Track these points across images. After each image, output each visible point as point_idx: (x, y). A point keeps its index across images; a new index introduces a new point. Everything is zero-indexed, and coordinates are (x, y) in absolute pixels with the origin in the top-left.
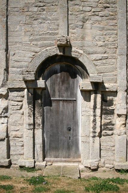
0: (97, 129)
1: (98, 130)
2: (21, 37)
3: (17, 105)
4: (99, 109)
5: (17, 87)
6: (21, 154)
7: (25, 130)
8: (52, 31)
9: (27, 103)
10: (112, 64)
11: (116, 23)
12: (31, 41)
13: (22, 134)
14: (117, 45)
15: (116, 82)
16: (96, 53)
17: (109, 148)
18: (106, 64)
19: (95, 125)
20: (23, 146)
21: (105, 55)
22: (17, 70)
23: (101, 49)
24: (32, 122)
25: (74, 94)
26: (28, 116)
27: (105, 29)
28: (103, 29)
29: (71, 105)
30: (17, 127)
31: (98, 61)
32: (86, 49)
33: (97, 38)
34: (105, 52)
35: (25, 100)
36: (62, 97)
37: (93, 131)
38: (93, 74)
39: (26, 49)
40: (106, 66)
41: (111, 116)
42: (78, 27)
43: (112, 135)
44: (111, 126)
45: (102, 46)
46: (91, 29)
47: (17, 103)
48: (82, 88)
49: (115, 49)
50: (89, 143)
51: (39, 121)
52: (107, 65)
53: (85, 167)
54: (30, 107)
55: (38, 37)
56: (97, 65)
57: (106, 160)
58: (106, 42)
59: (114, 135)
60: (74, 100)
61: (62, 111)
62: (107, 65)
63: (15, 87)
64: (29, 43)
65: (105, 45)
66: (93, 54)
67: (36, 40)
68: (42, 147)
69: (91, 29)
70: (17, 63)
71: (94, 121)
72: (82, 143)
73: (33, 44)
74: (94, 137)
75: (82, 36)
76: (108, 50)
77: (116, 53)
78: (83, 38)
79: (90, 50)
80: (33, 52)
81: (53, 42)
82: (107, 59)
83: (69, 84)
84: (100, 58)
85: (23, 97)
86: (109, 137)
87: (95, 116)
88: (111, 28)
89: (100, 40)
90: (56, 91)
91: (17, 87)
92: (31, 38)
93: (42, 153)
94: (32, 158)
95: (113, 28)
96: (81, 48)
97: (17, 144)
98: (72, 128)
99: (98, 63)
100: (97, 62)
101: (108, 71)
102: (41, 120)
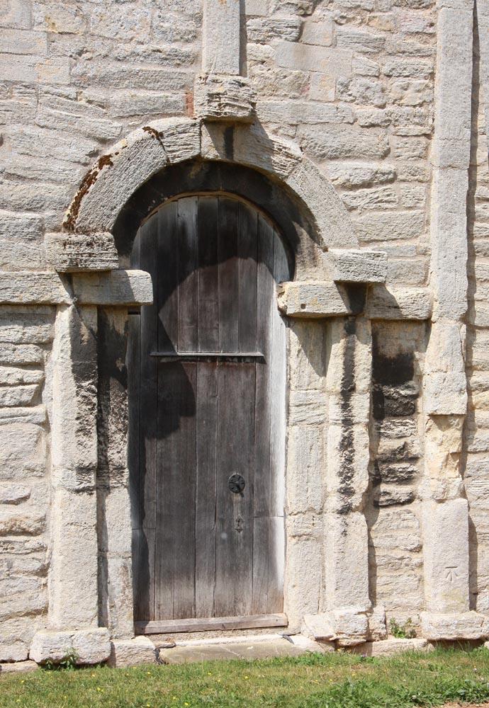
0: (356, 478)
1: (361, 481)
2: (32, 59)
3: (22, 383)
4: (363, 392)
5: (26, 298)
6: (37, 612)
7: (60, 495)
8: (175, 46)
9: (71, 374)
10: (411, 204)
11: (432, 25)
12: (82, 82)
13: (42, 514)
14: (430, 121)
15: (424, 282)
16: (346, 154)
17: (402, 558)
18: (387, 205)
19: (350, 460)
20: (43, 572)
21: (386, 166)
22: (14, 218)
23: (370, 139)
24: (92, 457)
25: (254, 332)
26: (75, 429)
27: (389, 49)
28: (377, 48)
29: (240, 381)
30: (17, 484)
31: (358, 192)
32: (313, 135)
33: (354, 90)
34: (385, 155)
35: (60, 360)
36: (208, 344)
37: (343, 485)
38: (342, 246)
39: (59, 119)
40: (388, 213)
41: (405, 425)
42: (279, 34)
43: (410, 501)
44: (404, 465)
45: (373, 125)
46: (334, 45)
47: (18, 373)
48: (303, 306)
49: (423, 139)
50: (320, 539)
51: (119, 452)
52: (392, 209)
53: (318, 640)
54: (83, 393)
55: (113, 67)
56: (352, 209)
57: (391, 607)
58: (389, 108)
59: (416, 501)
60: (254, 358)
61: (208, 408)
62: (392, 209)
63: (15, 300)
64: (72, 91)
65: (387, 123)
66: (336, 158)
67: (103, 81)
68: (129, 568)
69: (334, 45)
70: (14, 183)
71: (347, 443)
72: (294, 541)
73: (90, 102)
74: (345, 511)
75: (298, 77)
76: (395, 141)
77: (425, 157)
78: (301, 87)
79: (333, 142)
80: (89, 136)
81: (174, 98)
82: (391, 181)
83: (236, 289)
84: (367, 178)
85: (47, 345)
86: (398, 509)
87: (347, 423)
88: (412, 44)
89: (366, 100)
90: (180, 318)
91: (24, 300)
92: (78, 70)
93: (131, 596)
94: (96, 622)
95: (419, 46)
96: (291, 132)
97: (18, 564)
98: (246, 480)
99: (360, 197)
100: (351, 193)
101: (394, 235)
102: (126, 448)
